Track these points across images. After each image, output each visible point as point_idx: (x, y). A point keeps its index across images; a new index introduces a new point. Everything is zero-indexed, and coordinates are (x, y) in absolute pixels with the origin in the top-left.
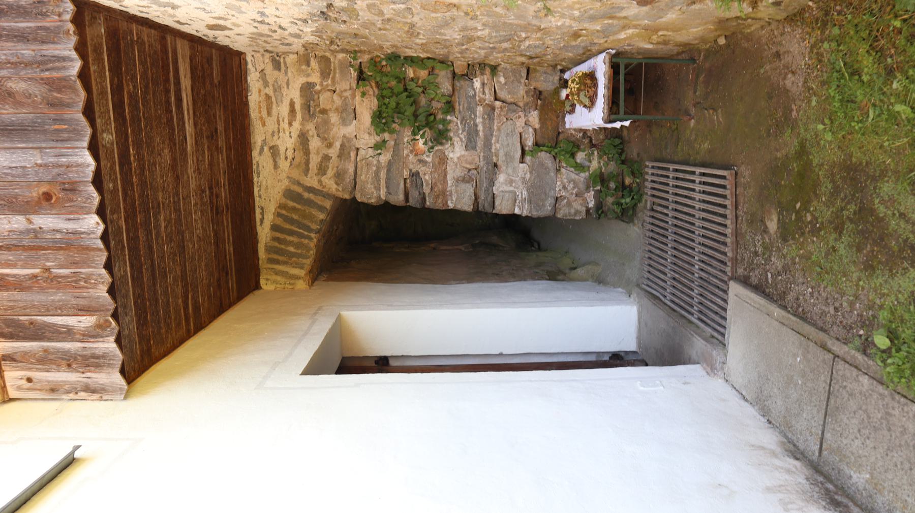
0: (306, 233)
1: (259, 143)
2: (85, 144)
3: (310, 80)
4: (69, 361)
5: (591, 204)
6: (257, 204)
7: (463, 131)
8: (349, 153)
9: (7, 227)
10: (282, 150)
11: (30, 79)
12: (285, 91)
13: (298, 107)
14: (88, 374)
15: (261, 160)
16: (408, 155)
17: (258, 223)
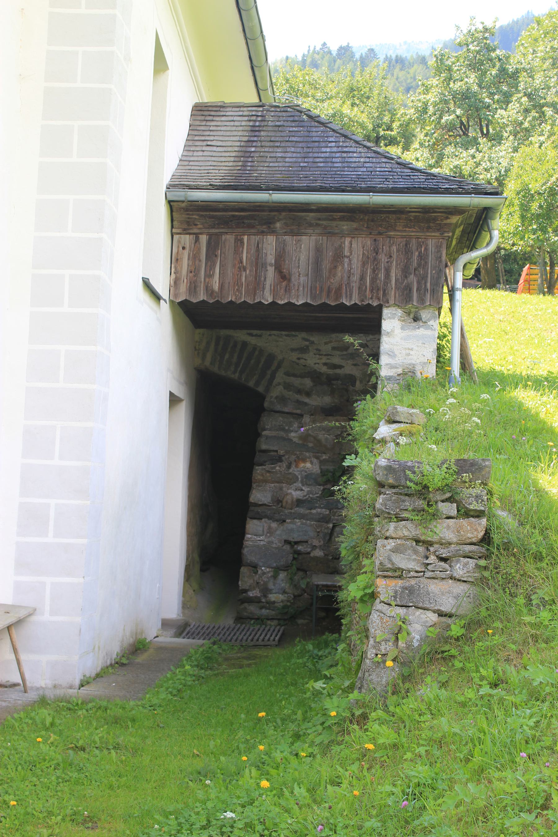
0: (239, 369)
1: (312, 339)
2: (309, 301)
3: (358, 383)
4: (194, 271)
5: (251, 594)
6: (264, 332)
7: (311, 498)
8: (299, 409)
9: (269, 253)
10: (305, 356)
11: (342, 278)
12: (350, 362)
13: (338, 371)
14: (185, 280)
15: (299, 339)
16: (295, 454)
17: (249, 331)
